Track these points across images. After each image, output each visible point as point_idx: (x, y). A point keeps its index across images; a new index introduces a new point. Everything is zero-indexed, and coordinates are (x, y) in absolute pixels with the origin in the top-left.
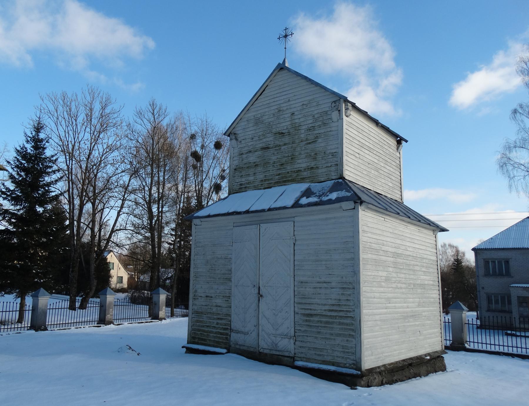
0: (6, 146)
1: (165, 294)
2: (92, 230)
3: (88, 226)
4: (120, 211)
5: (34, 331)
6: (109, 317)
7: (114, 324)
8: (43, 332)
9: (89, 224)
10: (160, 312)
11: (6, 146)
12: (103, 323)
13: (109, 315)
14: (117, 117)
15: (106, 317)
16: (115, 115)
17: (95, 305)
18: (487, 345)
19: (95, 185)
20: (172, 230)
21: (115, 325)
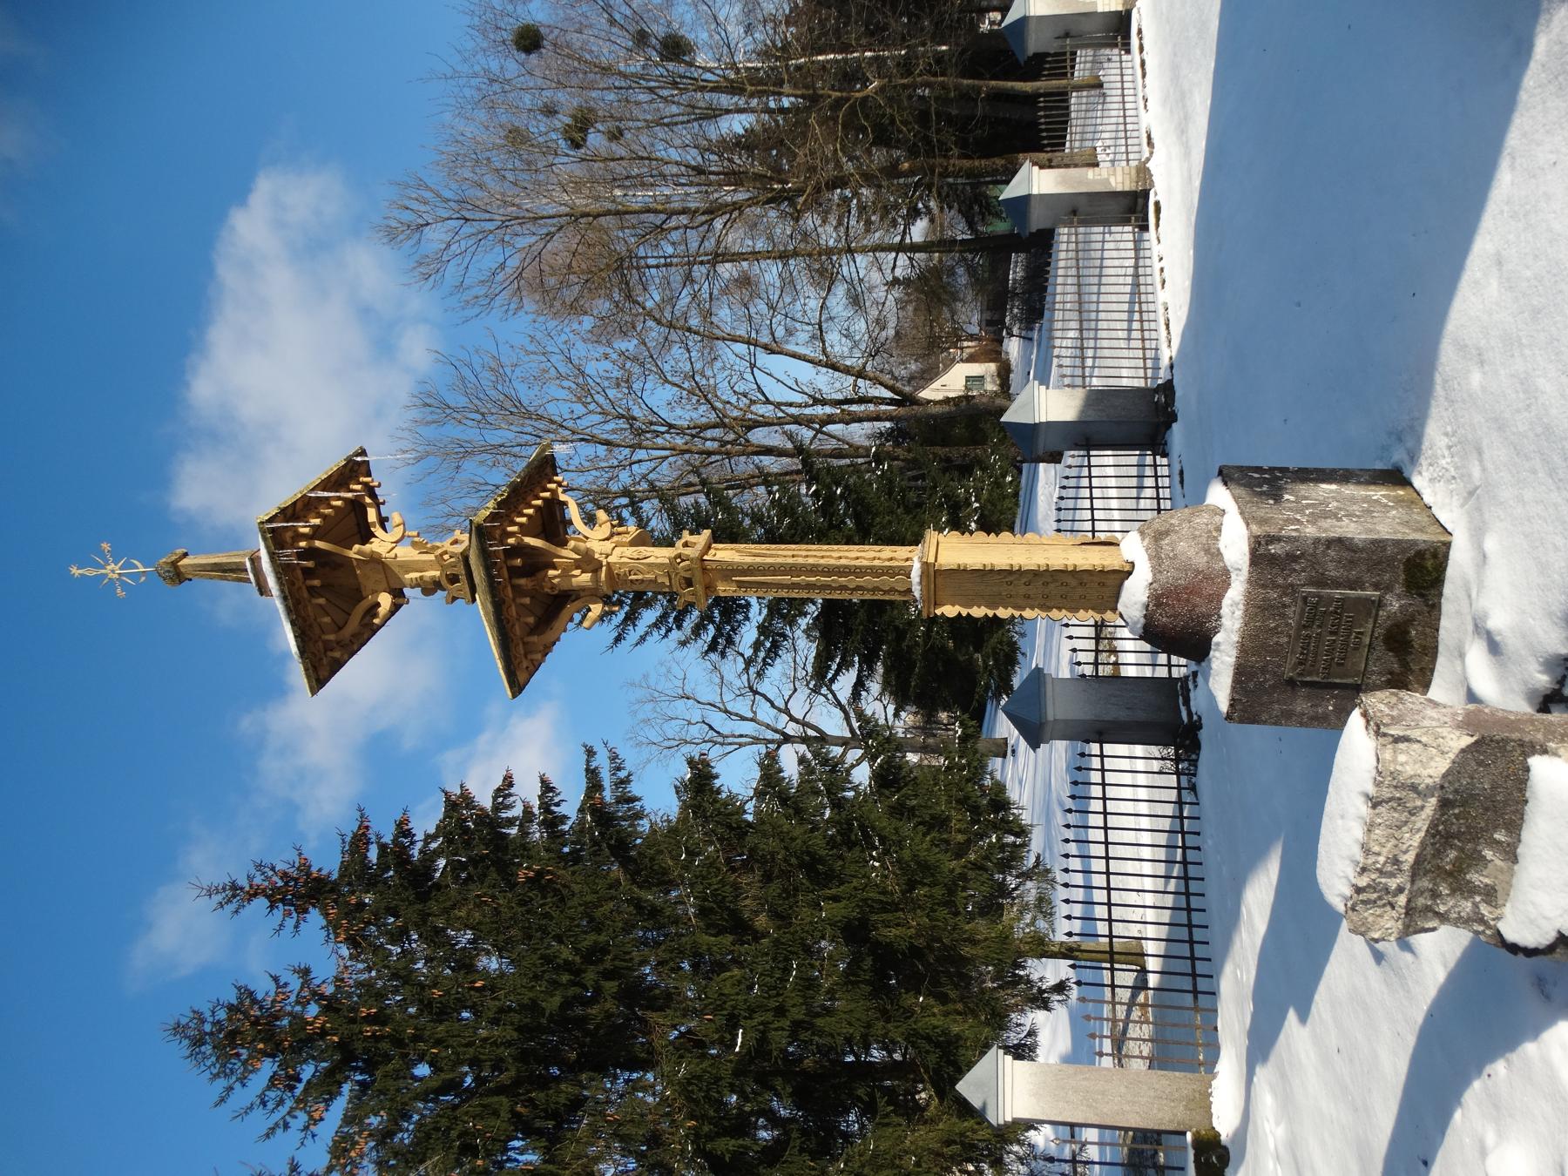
0: (633, 684)
1: (1030, 172)
2: (830, 420)
3: (819, 431)
4: (766, 347)
5: (1174, 425)
6: (1120, 179)
7: (1148, 160)
8: (1178, 394)
9: (813, 429)
10: (1100, 10)
11: (633, 684)
12: (1140, 201)
13: (1112, 180)
14: (470, 366)
15: (1119, 188)
16: (467, 372)
17: (1096, 763)
18: (1117, 990)
19: (695, 428)
20: (824, 221)
21: (1151, 153)
